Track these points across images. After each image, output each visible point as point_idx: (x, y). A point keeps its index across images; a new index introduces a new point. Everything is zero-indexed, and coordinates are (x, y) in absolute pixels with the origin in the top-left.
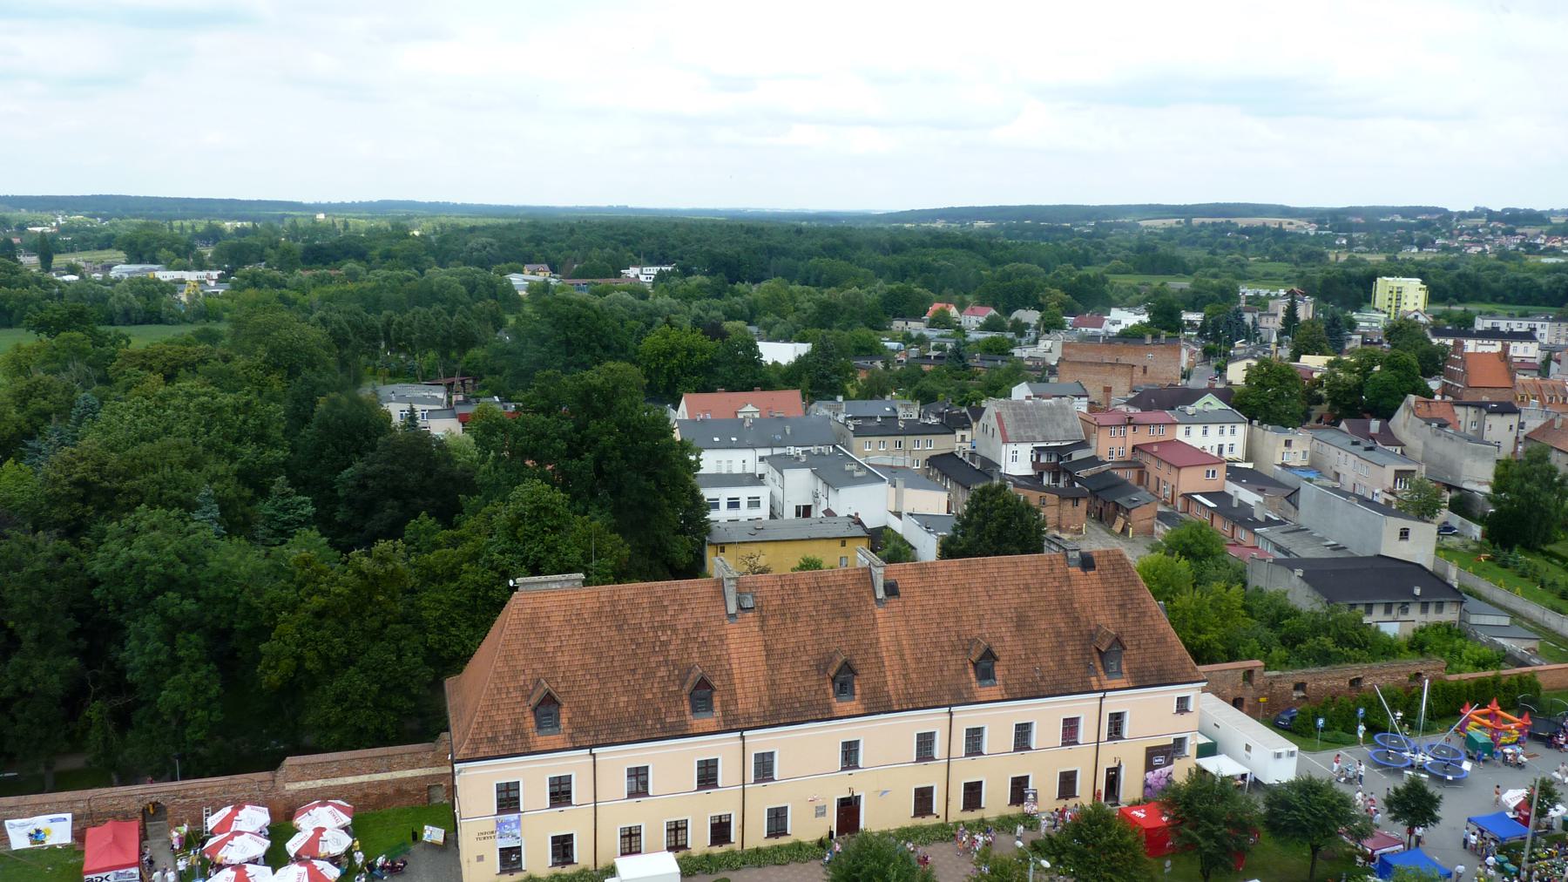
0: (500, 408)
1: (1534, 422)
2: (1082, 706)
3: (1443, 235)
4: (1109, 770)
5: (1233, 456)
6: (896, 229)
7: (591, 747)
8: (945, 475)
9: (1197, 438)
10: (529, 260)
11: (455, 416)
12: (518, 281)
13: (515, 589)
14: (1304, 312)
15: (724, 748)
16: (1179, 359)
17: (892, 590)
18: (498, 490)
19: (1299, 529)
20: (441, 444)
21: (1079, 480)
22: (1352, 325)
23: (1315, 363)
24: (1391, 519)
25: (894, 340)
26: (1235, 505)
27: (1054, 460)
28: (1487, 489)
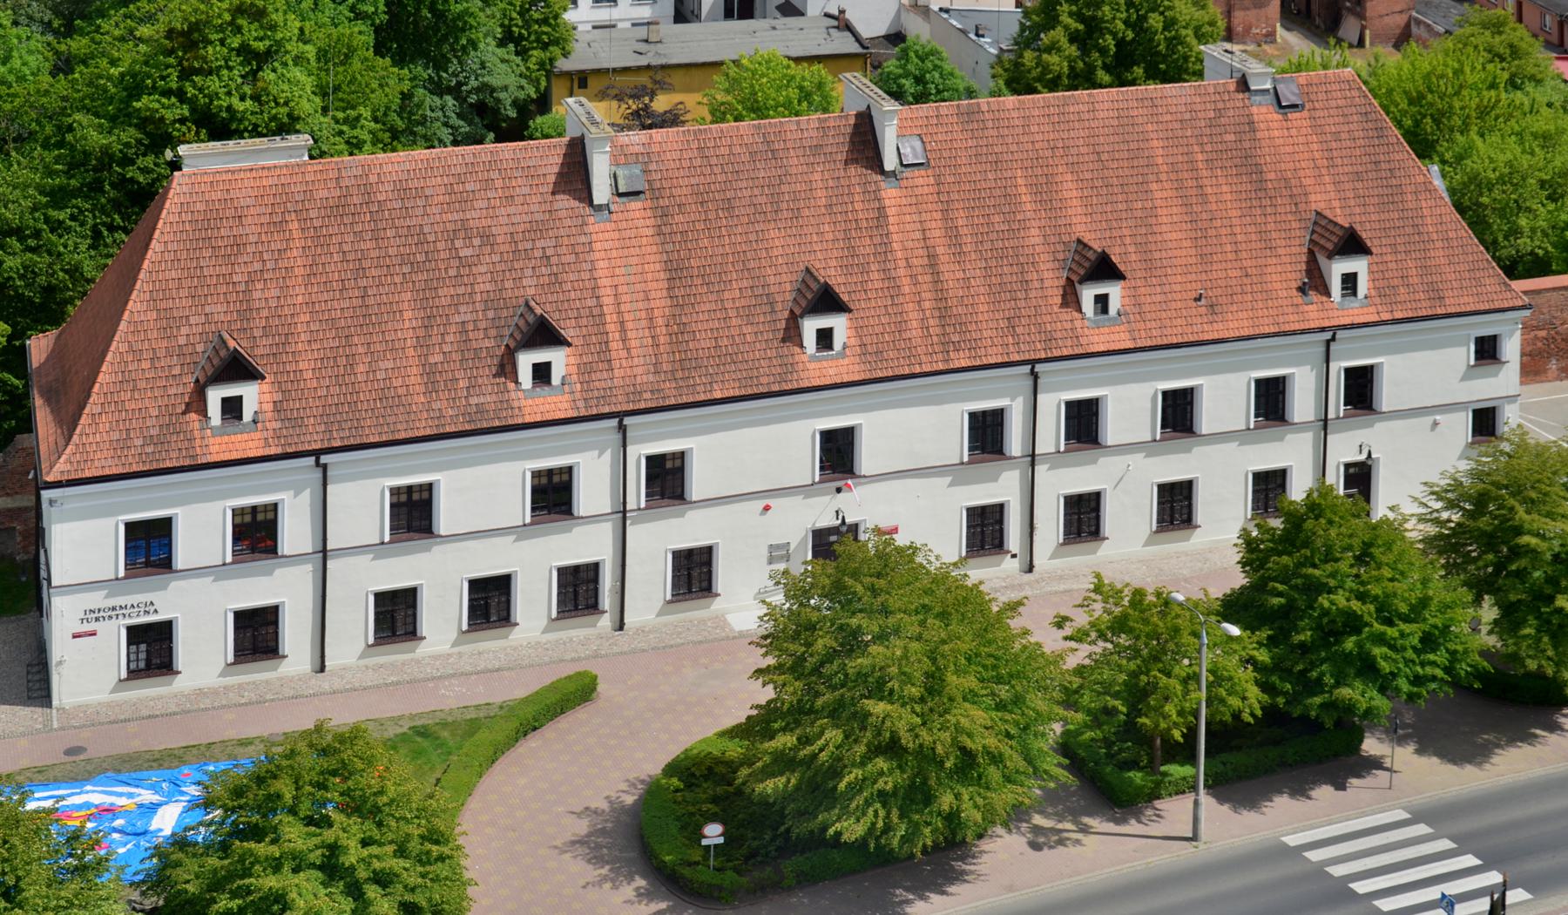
1: (1471, 610)
13: (175, 165)
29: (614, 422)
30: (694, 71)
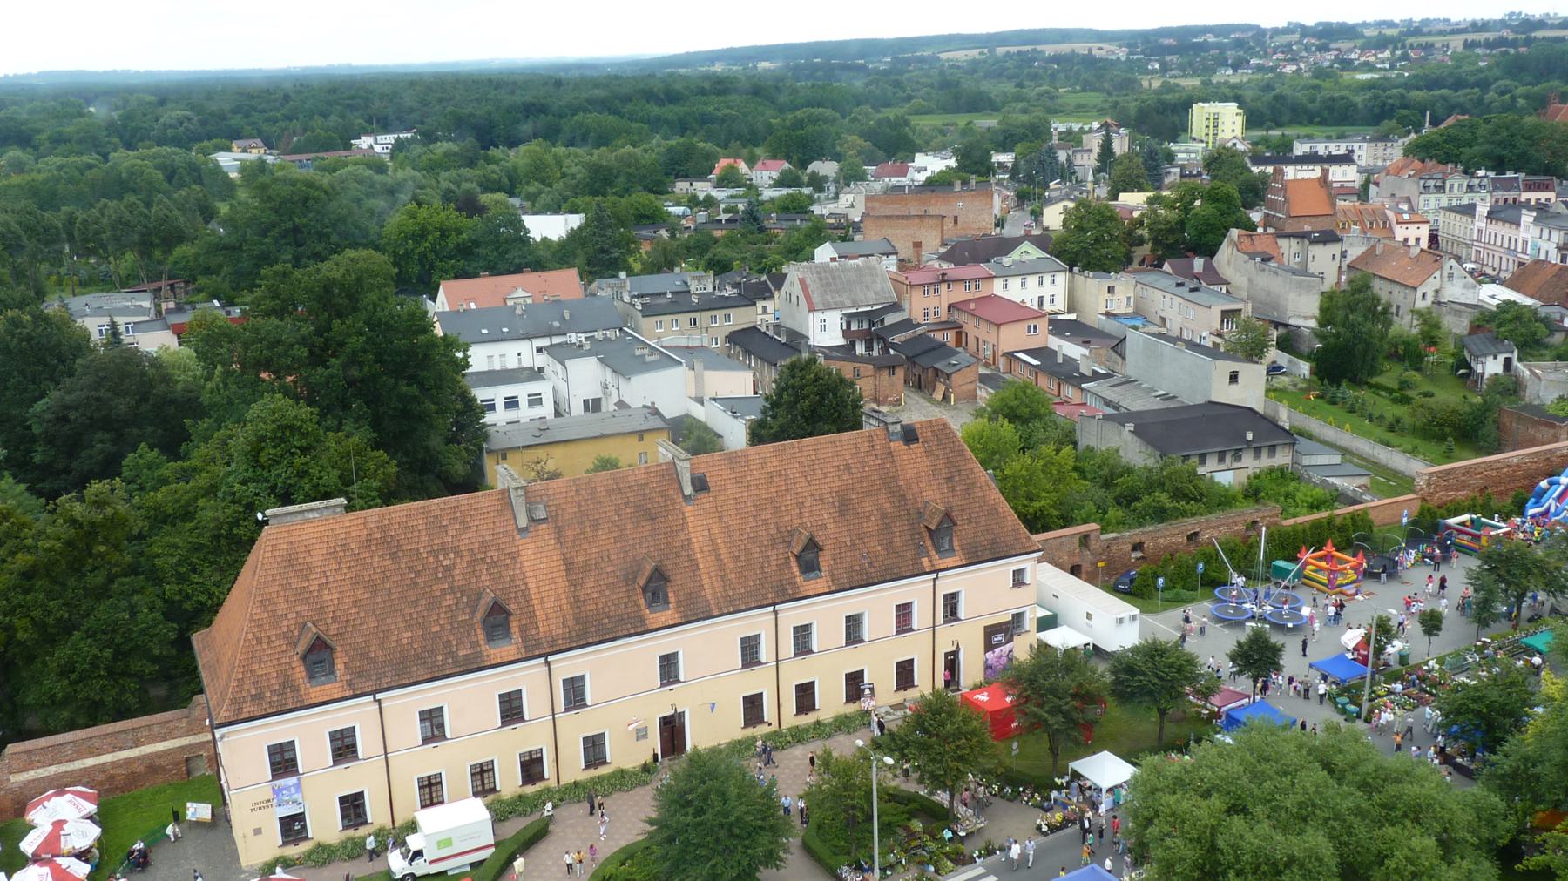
1: (1355, 252)
2: (917, 592)
3: (1257, 55)
4: (947, 655)
5: (1055, 308)
6: (671, 75)
7: (374, 693)
8: (748, 352)
9: (1015, 291)
10: (236, 135)
11: (168, 327)
12: (229, 161)
14: (1120, 146)
15: (529, 679)
16: (992, 206)
17: (700, 485)
18: (229, 410)
19: (1128, 382)
20: (154, 362)
21: (894, 346)
22: (1170, 157)
23: (1134, 201)
24: (1219, 363)
25: (678, 204)
26: (1060, 360)
27: (866, 326)
28: (1313, 324)
30: (572, 447)
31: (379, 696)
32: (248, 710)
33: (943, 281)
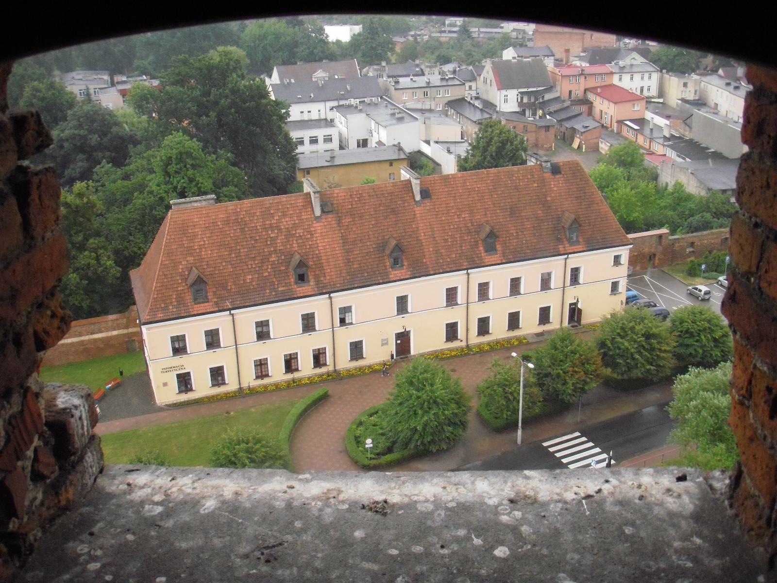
0: (146, 83)
2: (555, 266)
4: (571, 305)
5: (650, 94)
9: (626, 83)
15: (318, 305)
17: (425, 194)
18: (151, 139)
20: (110, 113)
27: (533, 100)
29: (327, 296)
31: (233, 312)
32: (160, 315)
33: (582, 74)
